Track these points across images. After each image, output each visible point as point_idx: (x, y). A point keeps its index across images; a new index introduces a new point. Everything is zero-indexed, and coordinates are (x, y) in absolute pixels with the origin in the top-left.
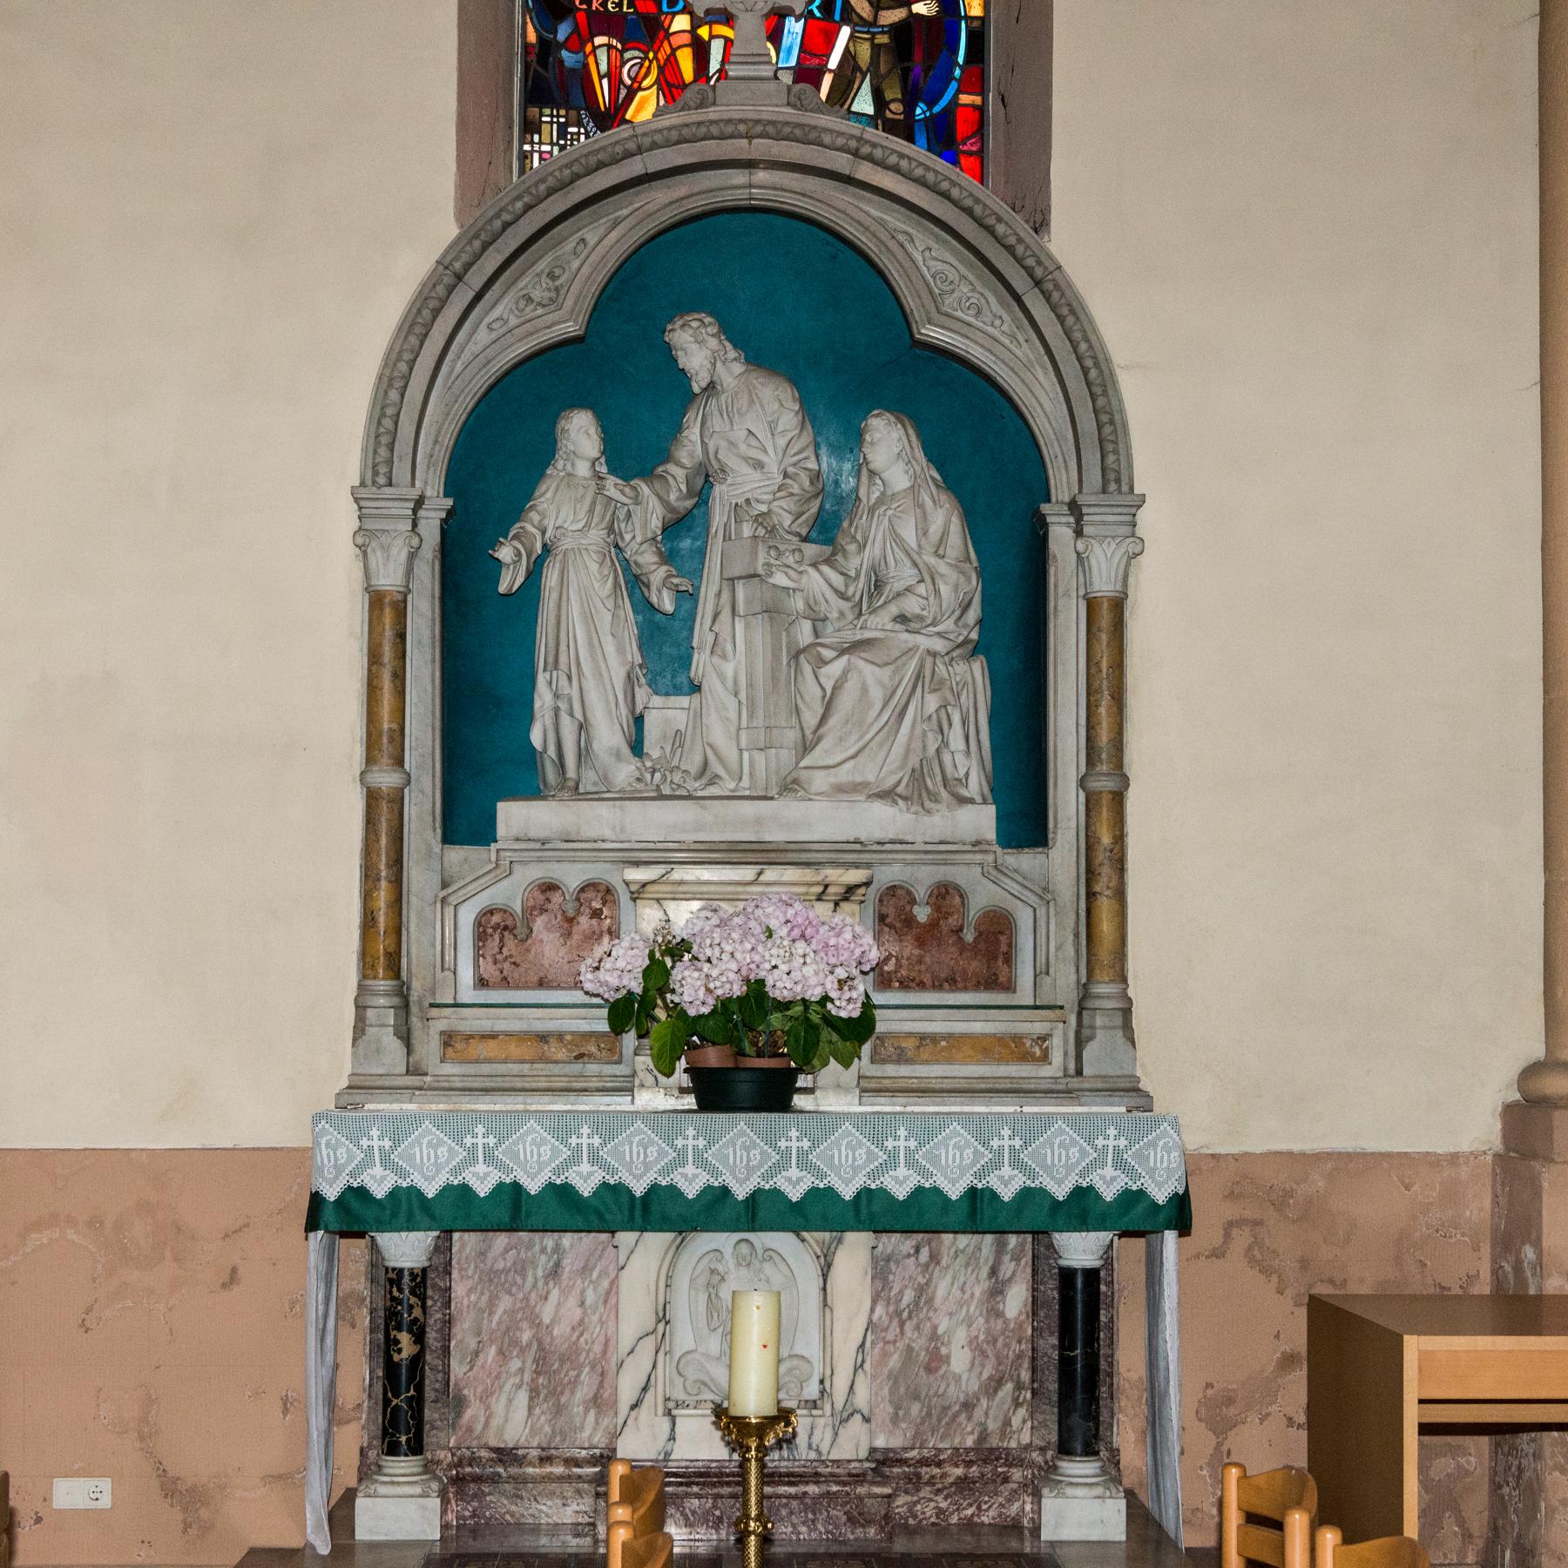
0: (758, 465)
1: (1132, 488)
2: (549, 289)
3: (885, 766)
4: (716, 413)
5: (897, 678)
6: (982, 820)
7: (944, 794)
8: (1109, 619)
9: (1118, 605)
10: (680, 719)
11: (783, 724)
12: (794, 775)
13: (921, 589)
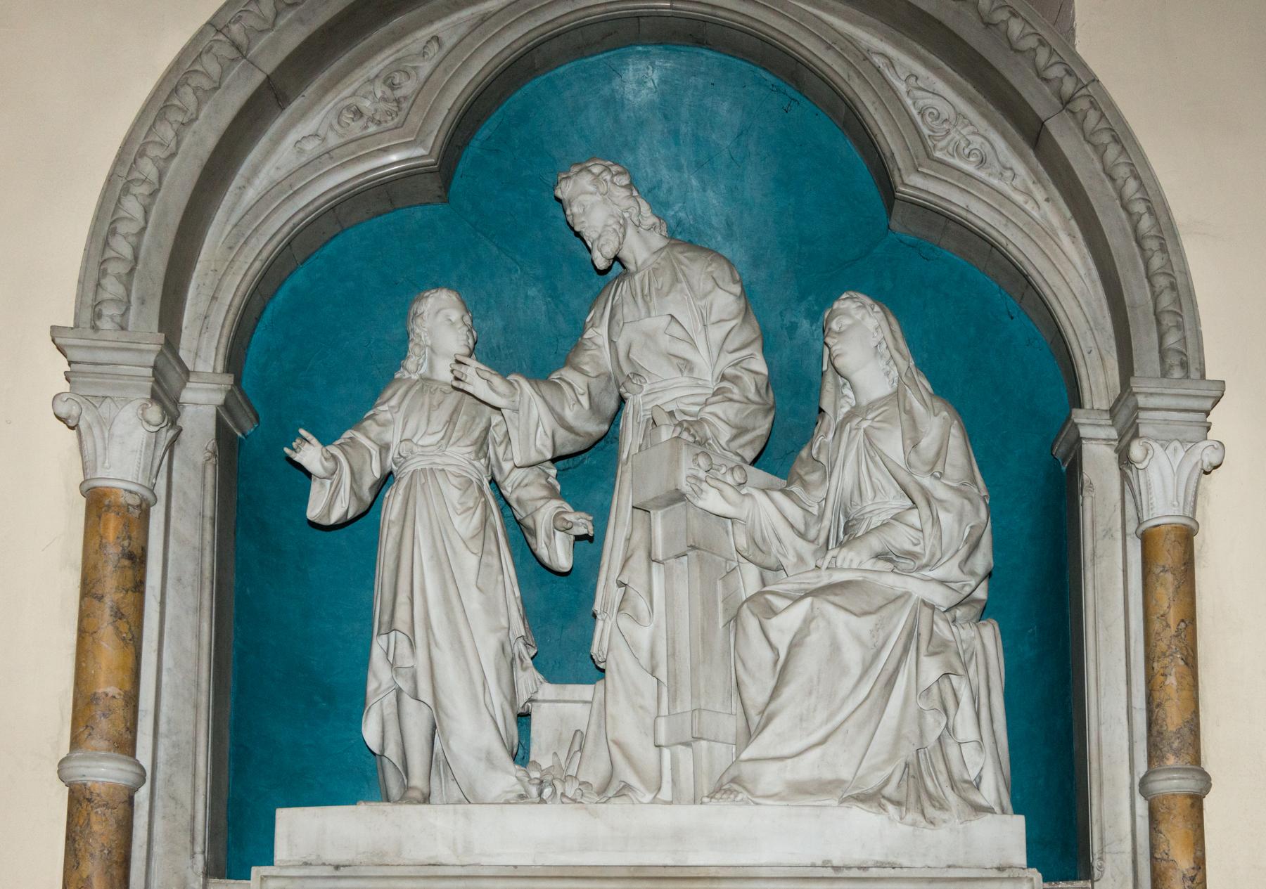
0: (686, 366)
1: (1203, 376)
2: (384, 99)
3: (870, 755)
4: (629, 299)
5: (882, 635)
6: (1007, 835)
7: (952, 797)
8: (1171, 556)
9: (1186, 536)
10: (579, 715)
11: (718, 708)
12: (733, 772)
13: (913, 518)
